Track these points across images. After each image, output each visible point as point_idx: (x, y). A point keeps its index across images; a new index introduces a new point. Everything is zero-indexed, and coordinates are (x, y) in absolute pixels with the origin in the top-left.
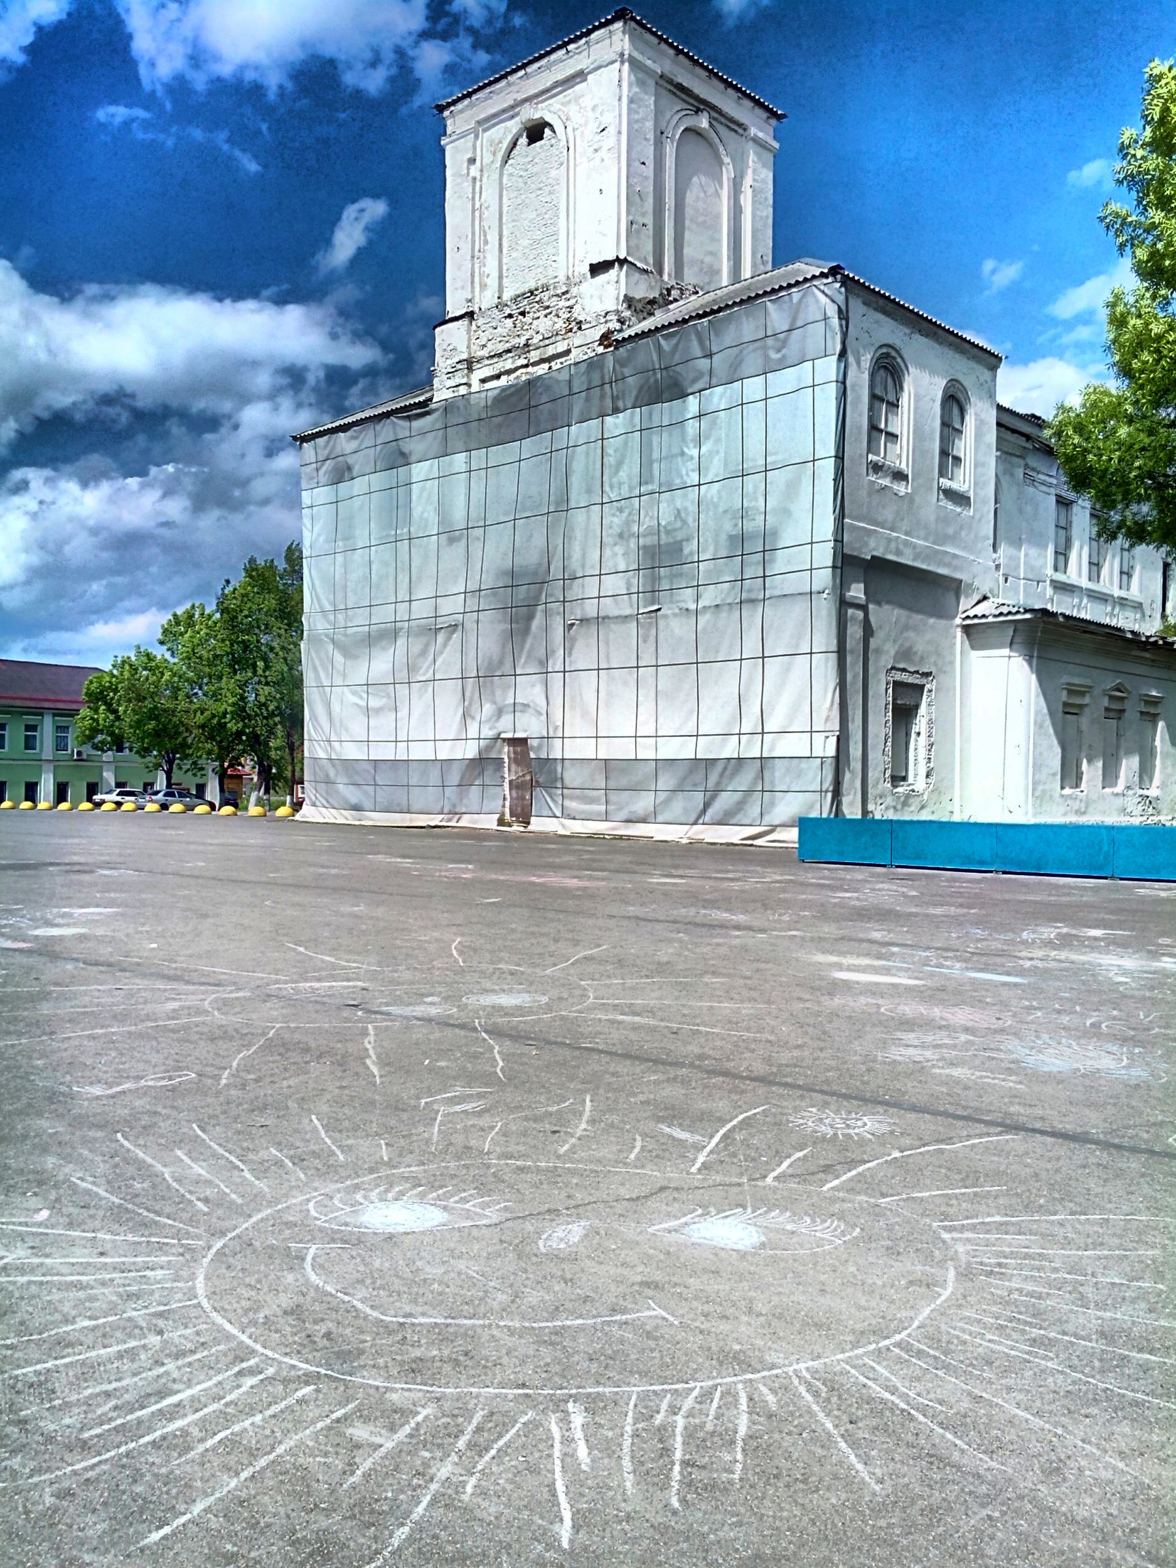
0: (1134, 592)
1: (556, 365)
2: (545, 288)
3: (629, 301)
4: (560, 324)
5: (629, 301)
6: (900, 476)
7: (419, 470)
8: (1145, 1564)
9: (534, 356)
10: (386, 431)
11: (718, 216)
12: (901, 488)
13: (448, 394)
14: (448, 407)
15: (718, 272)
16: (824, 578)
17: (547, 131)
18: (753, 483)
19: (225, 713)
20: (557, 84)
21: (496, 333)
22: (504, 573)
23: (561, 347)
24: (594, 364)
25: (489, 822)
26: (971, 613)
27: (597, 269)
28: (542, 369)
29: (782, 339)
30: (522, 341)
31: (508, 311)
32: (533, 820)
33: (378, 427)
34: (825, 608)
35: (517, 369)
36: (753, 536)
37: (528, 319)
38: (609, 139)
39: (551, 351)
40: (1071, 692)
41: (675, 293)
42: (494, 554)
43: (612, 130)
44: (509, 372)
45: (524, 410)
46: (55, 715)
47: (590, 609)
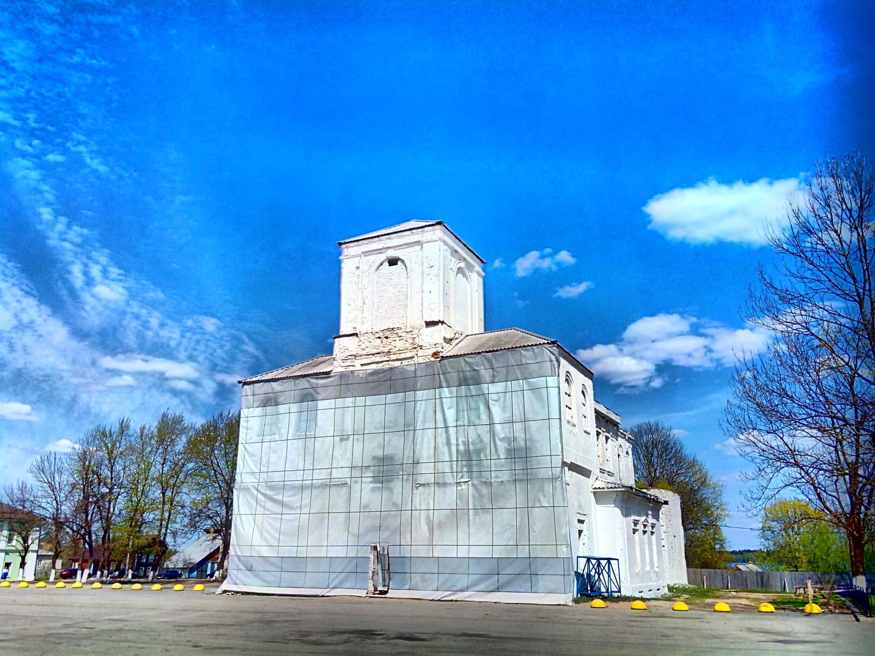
1: (405, 363)
7: (321, 404)
9: (393, 357)
10: (303, 383)
14: (342, 376)
17: (399, 263)
18: (518, 427)
20: (405, 244)
23: (409, 355)
24: (428, 365)
27: (429, 324)
28: (397, 364)
30: (386, 350)
31: (378, 335)
33: (297, 381)
35: (382, 362)
36: (519, 449)
37: (389, 340)
38: (434, 271)
42: (373, 448)
43: (436, 267)
44: (377, 363)
45: (388, 381)
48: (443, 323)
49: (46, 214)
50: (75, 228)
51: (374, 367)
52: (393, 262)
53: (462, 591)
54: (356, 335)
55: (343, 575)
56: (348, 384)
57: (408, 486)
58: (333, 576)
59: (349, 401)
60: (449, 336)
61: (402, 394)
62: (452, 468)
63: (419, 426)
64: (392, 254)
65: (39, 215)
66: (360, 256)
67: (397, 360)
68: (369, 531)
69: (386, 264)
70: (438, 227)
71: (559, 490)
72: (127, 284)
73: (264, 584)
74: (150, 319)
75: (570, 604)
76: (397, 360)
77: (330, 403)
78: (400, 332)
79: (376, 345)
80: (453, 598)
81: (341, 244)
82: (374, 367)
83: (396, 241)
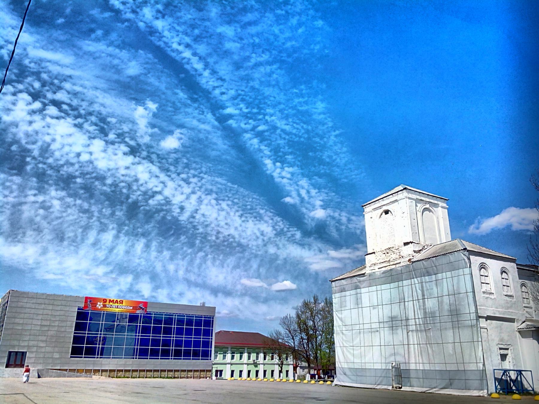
1: (397, 266)
2: (393, 247)
7: (363, 290)
8: (1, 308)
9: (392, 263)
11: (434, 227)
14: (370, 275)
15: (436, 239)
17: (389, 213)
22: (389, 317)
23: (398, 261)
24: (407, 266)
26: (519, 327)
27: (406, 244)
28: (394, 267)
37: (389, 254)
38: (405, 214)
41: (426, 247)
42: (386, 312)
44: (385, 267)
48: (412, 243)
49: (268, 162)
50: (286, 169)
51: (384, 269)
52: (387, 212)
53: (435, 388)
54: (374, 253)
55: (381, 378)
56: (373, 280)
57: (405, 332)
58: (377, 378)
59: (374, 288)
60: (417, 249)
61: (434, 276)
62: (427, 321)
63: (406, 300)
64: (385, 208)
65: (265, 165)
66: (372, 211)
67: (394, 265)
68: (391, 355)
69: (384, 214)
70: (404, 191)
71: (475, 332)
72: (321, 198)
73: (351, 381)
74: (341, 218)
75: (486, 396)
76: (394, 265)
77: (366, 290)
78: (393, 249)
79: (383, 258)
80: (430, 391)
81: (363, 206)
82: (384, 269)
83: (386, 201)
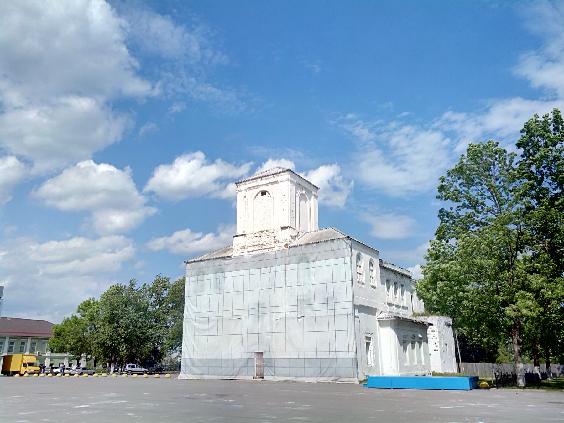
0: (404, 303)
1: (270, 250)
3: (291, 236)
4: (272, 240)
5: (291, 236)
6: (363, 283)
9: (264, 247)
12: (364, 286)
13: (238, 255)
14: (237, 258)
16: (350, 311)
19: (107, 339)
21: (251, 240)
23: (272, 246)
25: (251, 378)
27: (282, 228)
28: (266, 251)
29: (335, 251)
30: (261, 243)
31: (256, 235)
32: (265, 377)
34: (351, 318)
37: (262, 238)
39: (269, 246)
40: (404, 337)
45: (262, 260)
46: (10, 338)
47: (283, 315)
